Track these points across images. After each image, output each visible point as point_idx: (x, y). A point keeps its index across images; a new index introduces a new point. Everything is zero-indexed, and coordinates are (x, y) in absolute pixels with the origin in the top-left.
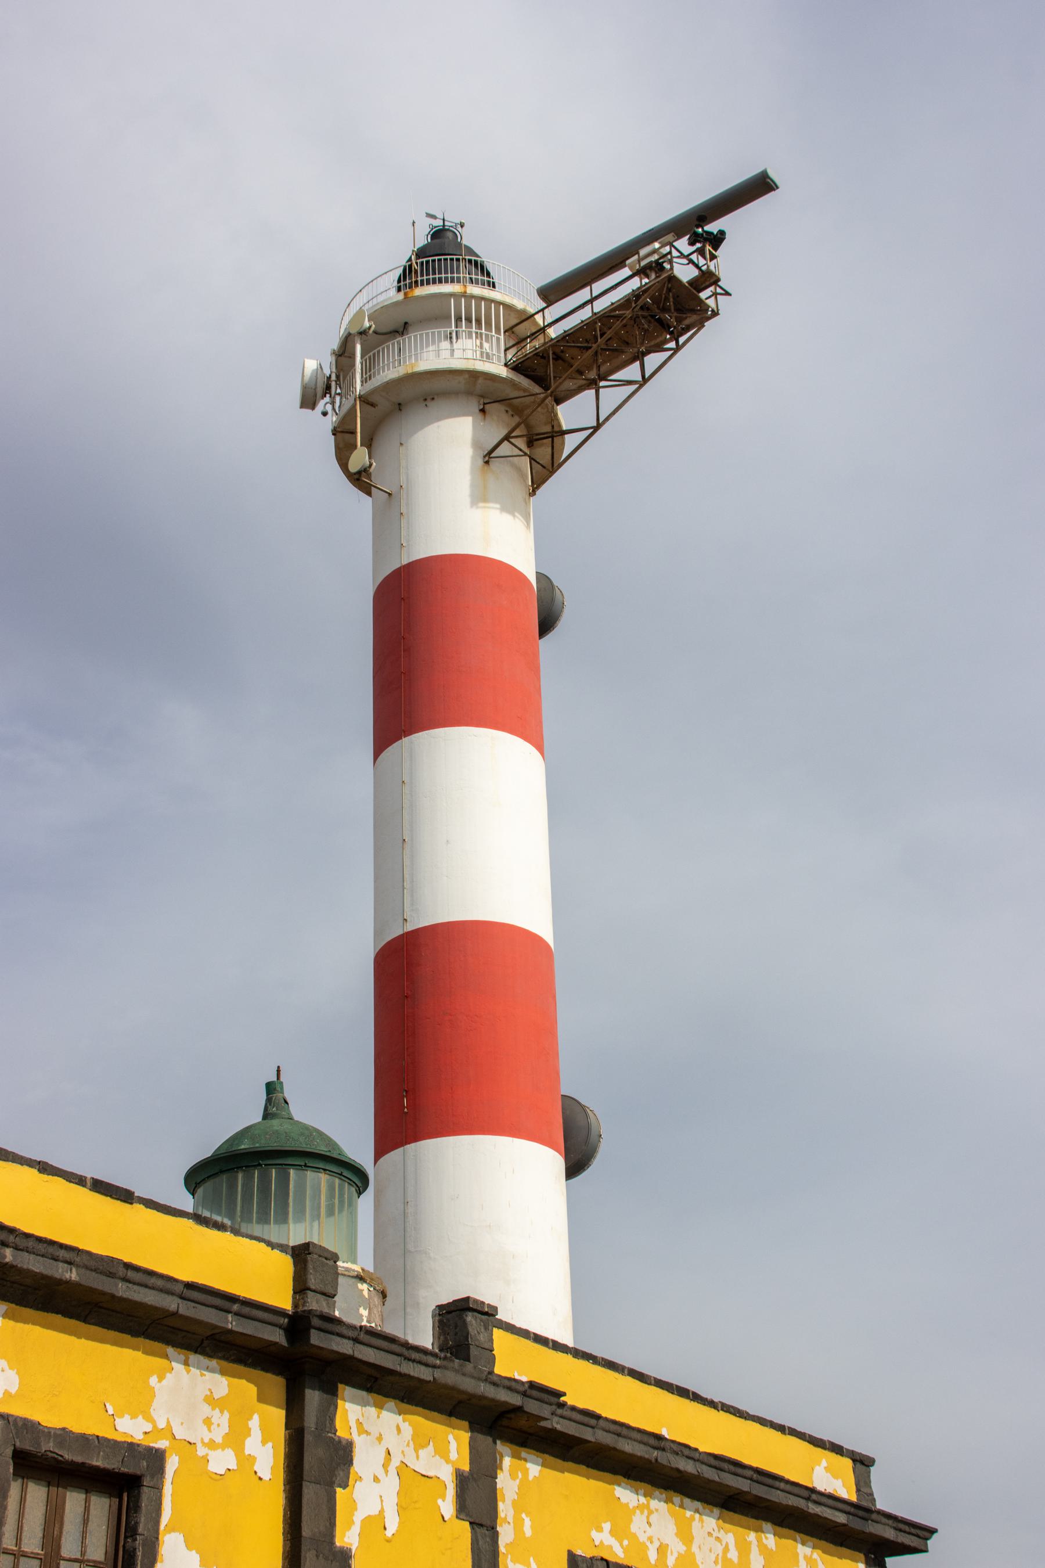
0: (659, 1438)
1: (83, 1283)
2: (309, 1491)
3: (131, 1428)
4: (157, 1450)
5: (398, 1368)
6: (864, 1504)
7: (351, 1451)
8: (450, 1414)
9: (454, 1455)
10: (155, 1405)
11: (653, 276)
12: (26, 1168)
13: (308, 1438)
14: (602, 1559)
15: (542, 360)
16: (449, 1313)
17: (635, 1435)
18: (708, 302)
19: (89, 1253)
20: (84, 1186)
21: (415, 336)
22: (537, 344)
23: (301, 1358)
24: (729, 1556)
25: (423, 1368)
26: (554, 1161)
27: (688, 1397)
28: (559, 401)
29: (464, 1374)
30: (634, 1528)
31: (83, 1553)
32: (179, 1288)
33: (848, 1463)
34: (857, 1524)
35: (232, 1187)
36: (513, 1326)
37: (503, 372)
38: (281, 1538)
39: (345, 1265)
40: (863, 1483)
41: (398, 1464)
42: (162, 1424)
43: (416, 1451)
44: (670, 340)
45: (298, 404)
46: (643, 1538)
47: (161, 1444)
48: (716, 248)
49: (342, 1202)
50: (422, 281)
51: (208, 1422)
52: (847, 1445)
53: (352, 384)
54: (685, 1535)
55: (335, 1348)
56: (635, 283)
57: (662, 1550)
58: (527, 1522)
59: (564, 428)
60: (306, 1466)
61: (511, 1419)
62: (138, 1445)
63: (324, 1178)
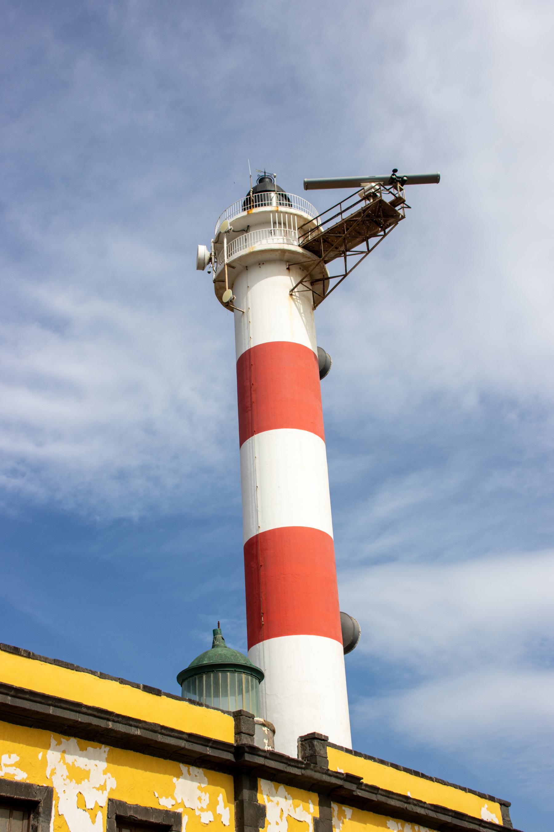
0: (407, 798)
3: (166, 804)
4: (178, 813)
5: (285, 770)
6: (507, 826)
7: (265, 810)
8: (309, 790)
10: (176, 792)
11: (372, 201)
12: (114, 681)
13: (245, 804)
15: (317, 243)
16: (305, 740)
17: (395, 797)
18: (399, 211)
19: (145, 722)
20: (140, 689)
21: (254, 233)
22: (315, 234)
25: (296, 769)
26: (339, 647)
27: (419, 776)
28: (326, 262)
29: (315, 771)
32: (185, 736)
33: (497, 805)
36: (336, 745)
37: (300, 250)
40: (505, 816)
41: (287, 815)
42: (179, 801)
43: (295, 808)
45: (196, 268)
47: (179, 810)
49: (252, 686)
50: (256, 205)
51: (199, 798)
52: (497, 796)
53: (224, 261)
55: (256, 761)
56: (363, 204)
60: (245, 818)
62: (170, 811)
63: (244, 676)
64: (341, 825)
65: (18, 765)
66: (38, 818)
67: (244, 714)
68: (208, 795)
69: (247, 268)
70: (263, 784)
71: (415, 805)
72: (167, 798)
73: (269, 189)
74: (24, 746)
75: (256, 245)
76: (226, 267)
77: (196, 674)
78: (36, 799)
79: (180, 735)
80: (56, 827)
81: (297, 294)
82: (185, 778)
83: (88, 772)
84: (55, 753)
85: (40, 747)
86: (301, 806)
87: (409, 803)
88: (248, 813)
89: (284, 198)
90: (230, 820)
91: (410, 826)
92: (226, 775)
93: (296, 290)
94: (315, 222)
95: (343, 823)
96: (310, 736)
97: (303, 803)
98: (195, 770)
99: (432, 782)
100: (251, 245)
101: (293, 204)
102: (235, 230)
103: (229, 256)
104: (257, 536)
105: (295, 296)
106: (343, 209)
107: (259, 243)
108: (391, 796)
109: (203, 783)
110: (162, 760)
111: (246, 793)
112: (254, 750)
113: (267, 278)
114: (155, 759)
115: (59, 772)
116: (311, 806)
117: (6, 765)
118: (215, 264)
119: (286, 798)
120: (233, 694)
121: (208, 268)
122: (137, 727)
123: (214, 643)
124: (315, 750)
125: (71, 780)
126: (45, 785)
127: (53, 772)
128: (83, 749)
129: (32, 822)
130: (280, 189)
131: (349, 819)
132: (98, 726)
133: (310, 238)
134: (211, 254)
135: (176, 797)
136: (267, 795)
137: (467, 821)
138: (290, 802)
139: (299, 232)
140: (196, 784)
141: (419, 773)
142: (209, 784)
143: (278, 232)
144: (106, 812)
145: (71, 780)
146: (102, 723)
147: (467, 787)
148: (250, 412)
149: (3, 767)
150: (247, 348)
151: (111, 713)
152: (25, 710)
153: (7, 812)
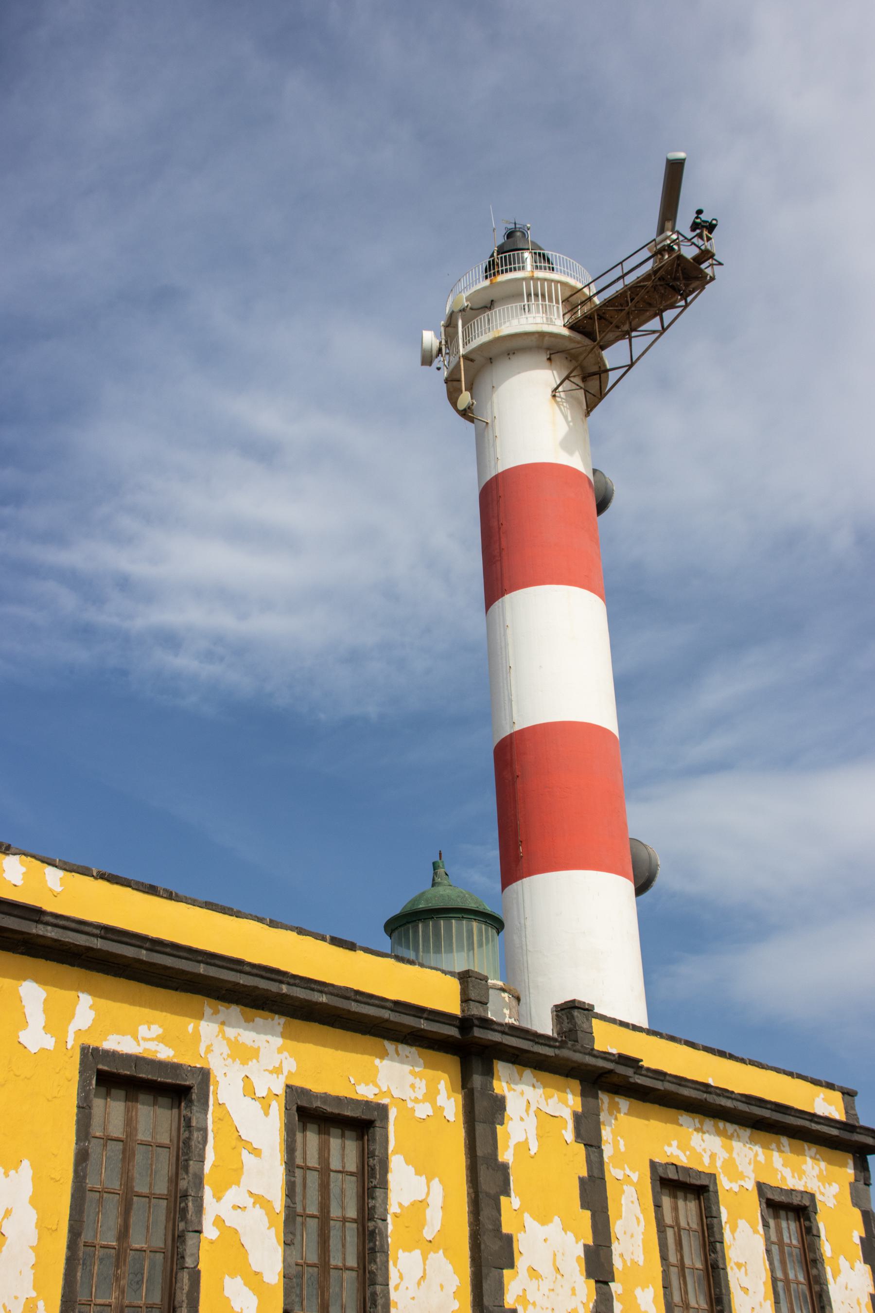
2: (480, 1128)
3: (366, 1092)
4: (383, 1105)
5: (532, 1049)
6: (851, 1122)
7: (504, 1102)
8: (567, 1076)
10: (379, 1076)
12: (289, 932)
14: (673, 1164)
15: (590, 321)
16: (562, 1010)
17: (690, 1084)
18: (706, 271)
19: (332, 985)
21: (499, 311)
22: (586, 309)
23: (471, 1047)
24: (759, 1158)
25: (547, 1048)
26: (625, 886)
28: (603, 348)
29: (575, 1051)
30: (693, 1143)
31: (344, 1167)
33: (838, 1095)
34: (846, 1135)
35: (416, 932)
37: (566, 332)
38: (464, 1157)
39: (493, 982)
41: (535, 1109)
42: (384, 1089)
43: (546, 1100)
44: (681, 300)
46: (699, 1150)
47: (385, 1101)
48: (710, 232)
49: (487, 938)
50: (506, 270)
51: (413, 1086)
52: (837, 1083)
53: (458, 352)
54: (730, 1150)
55: (490, 1038)
57: (713, 1156)
58: (622, 1142)
59: (608, 367)
60: (477, 1112)
63: (475, 924)
64: (613, 1121)
65: (161, 1039)
68: (424, 1082)
69: (491, 360)
70: (501, 1068)
71: (718, 1095)
72: (367, 1084)
73: (521, 247)
74: (169, 1015)
75: (503, 327)
76: (462, 360)
77: (409, 923)
78: (187, 1083)
79: (383, 1003)
81: (562, 394)
82: (392, 1060)
83: (258, 1050)
84: (211, 1024)
86: (556, 1097)
87: (710, 1093)
88: (481, 1105)
89: (542, 260)
90: (456, 1115)
91: (712, 1122)
92: (449, 1056)
93: (560, 389)
94: (586, 290)
95: (616, 1119)
97: (559, 1093)
98: (405, 1049)
99: (744, 1065)
100: (497, 328)
101: (554, 266)
102: (475, 307)
103: (465, 344)
104: (511, 735)
105: (560, 397)
106: (625, 272)
107: (507, 324)
108: (683, 1083)
109: (417, 1066)
110: (359, 1036)
111: (477, 1080)
112: (486, 1023)
113: (519, 373)
114: (349, 1034)
116: (570, 1097)
117: (144, 1039)
118: (447, 356)
119: (534, 1086)
120: (460, 948)
122: (321, 992)
123: (434, 880)
124: (576, 1023)
125: (234, 1061)
126: (198, 1066)
127: (209, 1049)
128: (247, 1020)
129: (184, 1112)
130: (535, 246)
131: (625, 1114)
132: (267, 990)
133: (579, 314)
134: (440, 343)
135: (380, 1083)
138: (540, 1091)
139: (564, 307)
140: (407, 1068)
142: (425, 1068)
143: (533, 308)
144: (284, 1102)
145: (234, 1061)
146: (273, 987)
149: (142, 1042)
150: (493, 474)
151: (285, 974)
153: (151, 1098)
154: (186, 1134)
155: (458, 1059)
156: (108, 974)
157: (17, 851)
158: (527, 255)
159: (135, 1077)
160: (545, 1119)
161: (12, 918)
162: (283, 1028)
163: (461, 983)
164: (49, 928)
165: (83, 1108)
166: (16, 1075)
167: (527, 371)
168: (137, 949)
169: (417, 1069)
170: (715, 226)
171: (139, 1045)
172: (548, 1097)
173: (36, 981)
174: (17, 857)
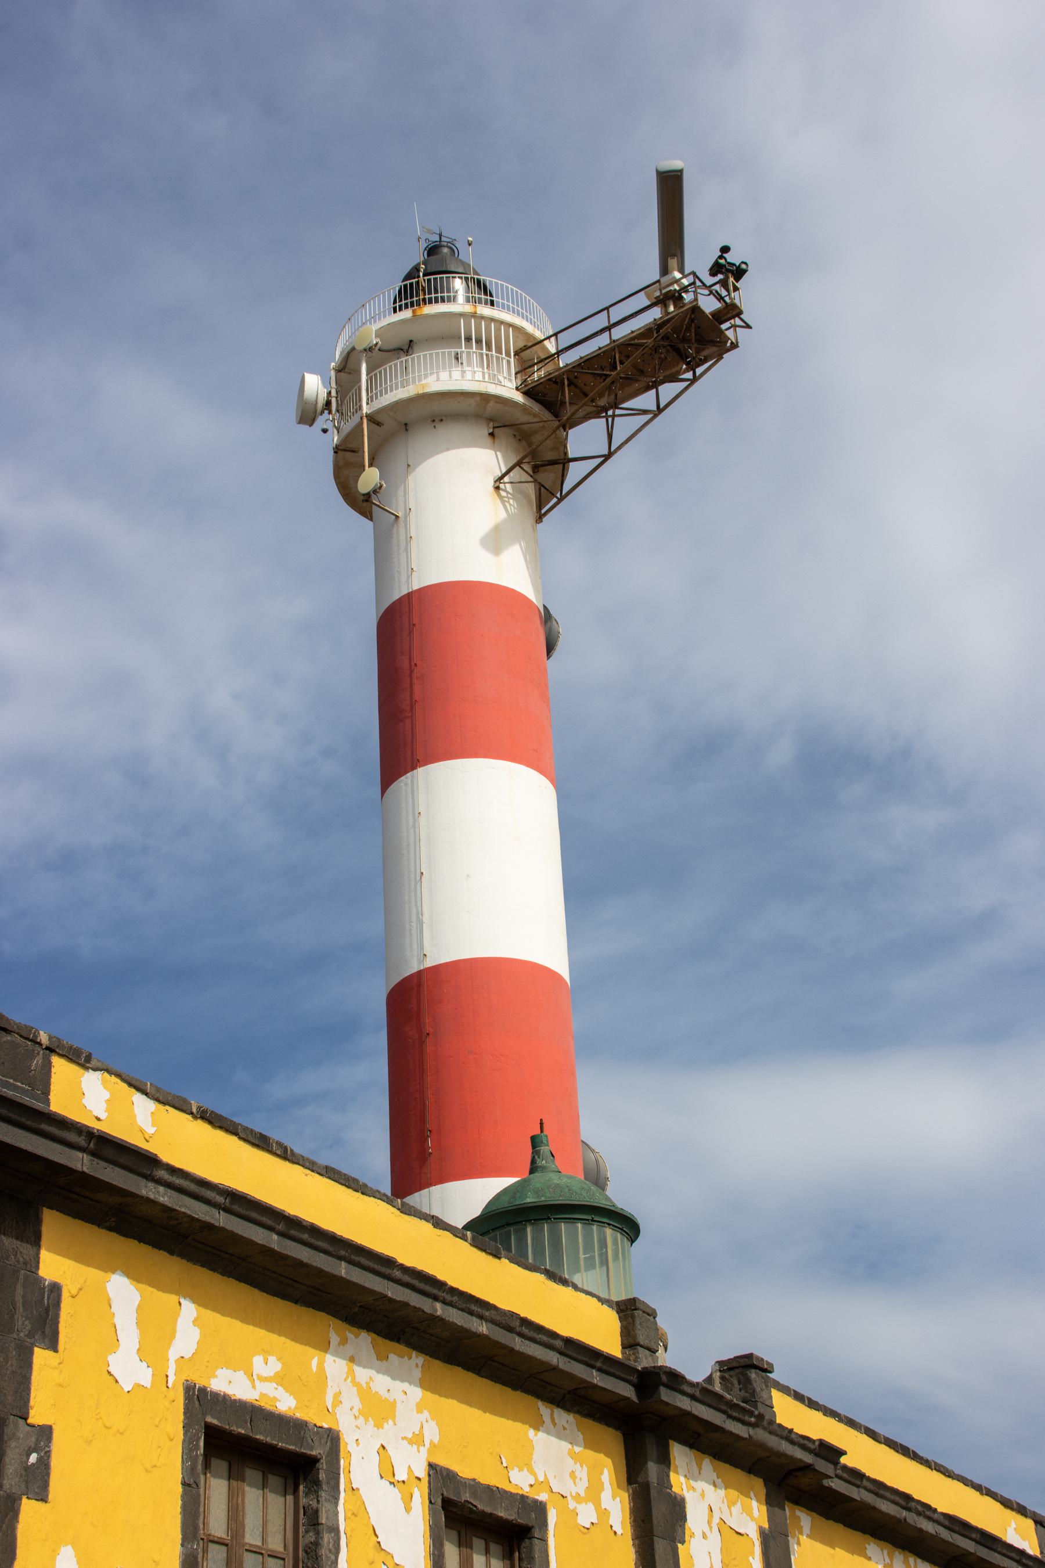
0: (908, 1497)
1: (491, 1336)
2: (660, 1546)
3: (520, 1482)
4: (541, 1502)
9: (756, 1513)
12: (423, 1222)
13: (653, 1493)
15: (554, 385)
16: (730, 1369)
17: (888, 1494)
18: (727, 333)
19: (495, 1308)
22: (550, 367)
29: (770, 1433)
32: (559, 1343)
33: (1030, 1523)
37: (519, 398)
42: (541, 1478)
43: (729, 1508)
44: (687, 371)
47: (543, 1497)
48: (737, 279)
51: (573, 1475)
52: (1031, 1507)
53: (360, 407)
55: (679, 1404)
59: (570, 456)
61: (796, 1476)
63: (609, 1232)
65: (279, 1379)
66: (317, 1492)
67: (641, 1307)
70: (679, 1453)
71: (919, 1513)
73: (453, 269)
74: (288, 1341)
76: (365, 421)
77: (508, 1224)
78: (314, 1453)
80: (349, 1515)
81: (509, 487)
82: (548, 1433)
83: (393, 1405)
85: (313, 1347)
86: (739, 1505)
87: (909, 1509)
88: (659, 1510)
89: (481, 289)
93: (506, 479)
95: (799, 1544)
96: (742, 1360)
99: (928, 1470)
102: (384, 348)
104: (420, 973)
105: (505, 490)
108: (881, 1492)
111: (652, 1469)
113: (448, 449)
115: (346, 1404)
119: (715, 1485)
121: (323, 421)
122: (481, 1317)
123: (533, 1161)
126: (326, 1426)
127: (337, 1401)
128: (382, 1357)
129: (303, 1501)
131: (808, 1536)
134: (329, 393)
136: (685, 1476)
137: (999, 1553)
138: (722, 1492)
140: (565, 1446)
141: (908, 1449)
142: (585, 1448)
144: (426, 1491)
145: (367, 1420)
147: (984, 1483)
148: (408, 722)
149: (257, 1382)
150: (405, 591)
151: (441, 1285)
152: (299, 1264)
154: (311, 1537)
155: (619, 1435)
156: (214, 1270)
157: (99, 1065)
158: (458, 284)
159: (250, 1437)
160: (731, 1534)
161: (117, 1169)
162: (422, 1372)
163: (620, 1318)
164: (161, 1189)
165: (189, 1485)
166: (106, 1427)
167: (458, 447)
168: (267, 1232)
169: (577, 1449)
170: (744, 272)
171: (254, 1387)
172: (731, 1504)
173: (128, 1275)
174: (98, 1073)
